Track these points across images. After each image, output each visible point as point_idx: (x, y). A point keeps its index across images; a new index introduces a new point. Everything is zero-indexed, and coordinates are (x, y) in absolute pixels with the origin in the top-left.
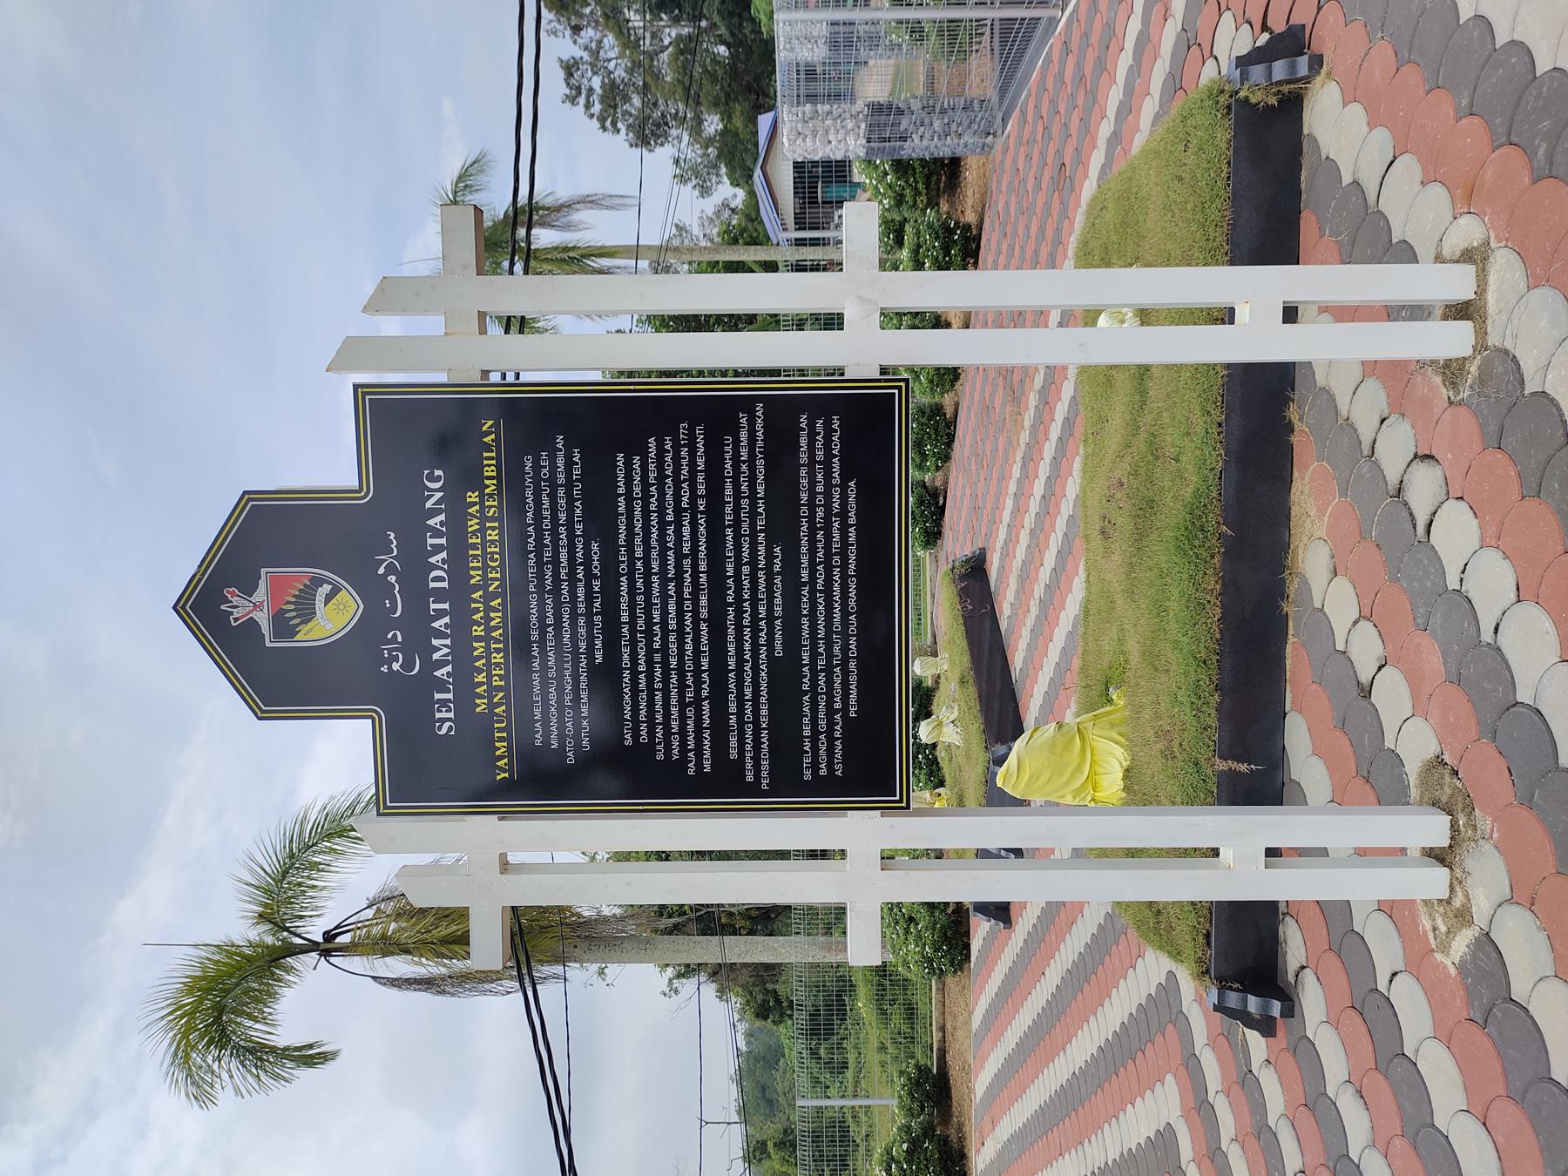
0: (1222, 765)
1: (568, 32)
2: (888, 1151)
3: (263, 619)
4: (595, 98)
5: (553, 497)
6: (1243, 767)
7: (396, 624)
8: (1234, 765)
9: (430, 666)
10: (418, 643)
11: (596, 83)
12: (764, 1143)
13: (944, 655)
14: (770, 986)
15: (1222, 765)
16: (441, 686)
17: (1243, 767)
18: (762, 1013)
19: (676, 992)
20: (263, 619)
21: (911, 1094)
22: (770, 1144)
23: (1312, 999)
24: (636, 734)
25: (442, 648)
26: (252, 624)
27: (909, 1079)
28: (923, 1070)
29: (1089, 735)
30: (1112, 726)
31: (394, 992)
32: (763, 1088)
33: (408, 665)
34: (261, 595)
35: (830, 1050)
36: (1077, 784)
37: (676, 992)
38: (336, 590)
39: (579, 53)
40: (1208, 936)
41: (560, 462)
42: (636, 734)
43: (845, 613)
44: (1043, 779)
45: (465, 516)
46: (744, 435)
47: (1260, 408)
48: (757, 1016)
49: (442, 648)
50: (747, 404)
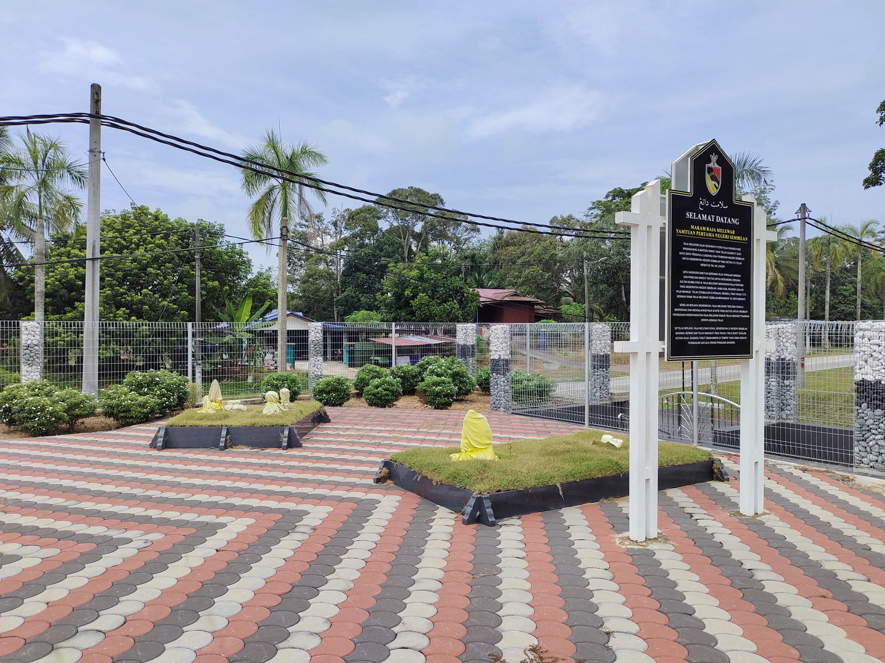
0: (558, 485)
1: (334, 220)
3: (711, 165)
4: (304, 229)
6: (561, 493)
8: (560, 488)
9: (701, 212)
10: (708, 211)
11: (311, 230)
16: (697, 216)
17: (561, 493)
20: (711, 165)
24: (686, 274)
25: (704, 217)
26: (710, 162)
33: (702, 207)
36: (473, 443)
39: (325, 222)
40: (500, 491)
42: (686, 274)
44: (475, 430)
49: (704, 217)
50: (749, 314)
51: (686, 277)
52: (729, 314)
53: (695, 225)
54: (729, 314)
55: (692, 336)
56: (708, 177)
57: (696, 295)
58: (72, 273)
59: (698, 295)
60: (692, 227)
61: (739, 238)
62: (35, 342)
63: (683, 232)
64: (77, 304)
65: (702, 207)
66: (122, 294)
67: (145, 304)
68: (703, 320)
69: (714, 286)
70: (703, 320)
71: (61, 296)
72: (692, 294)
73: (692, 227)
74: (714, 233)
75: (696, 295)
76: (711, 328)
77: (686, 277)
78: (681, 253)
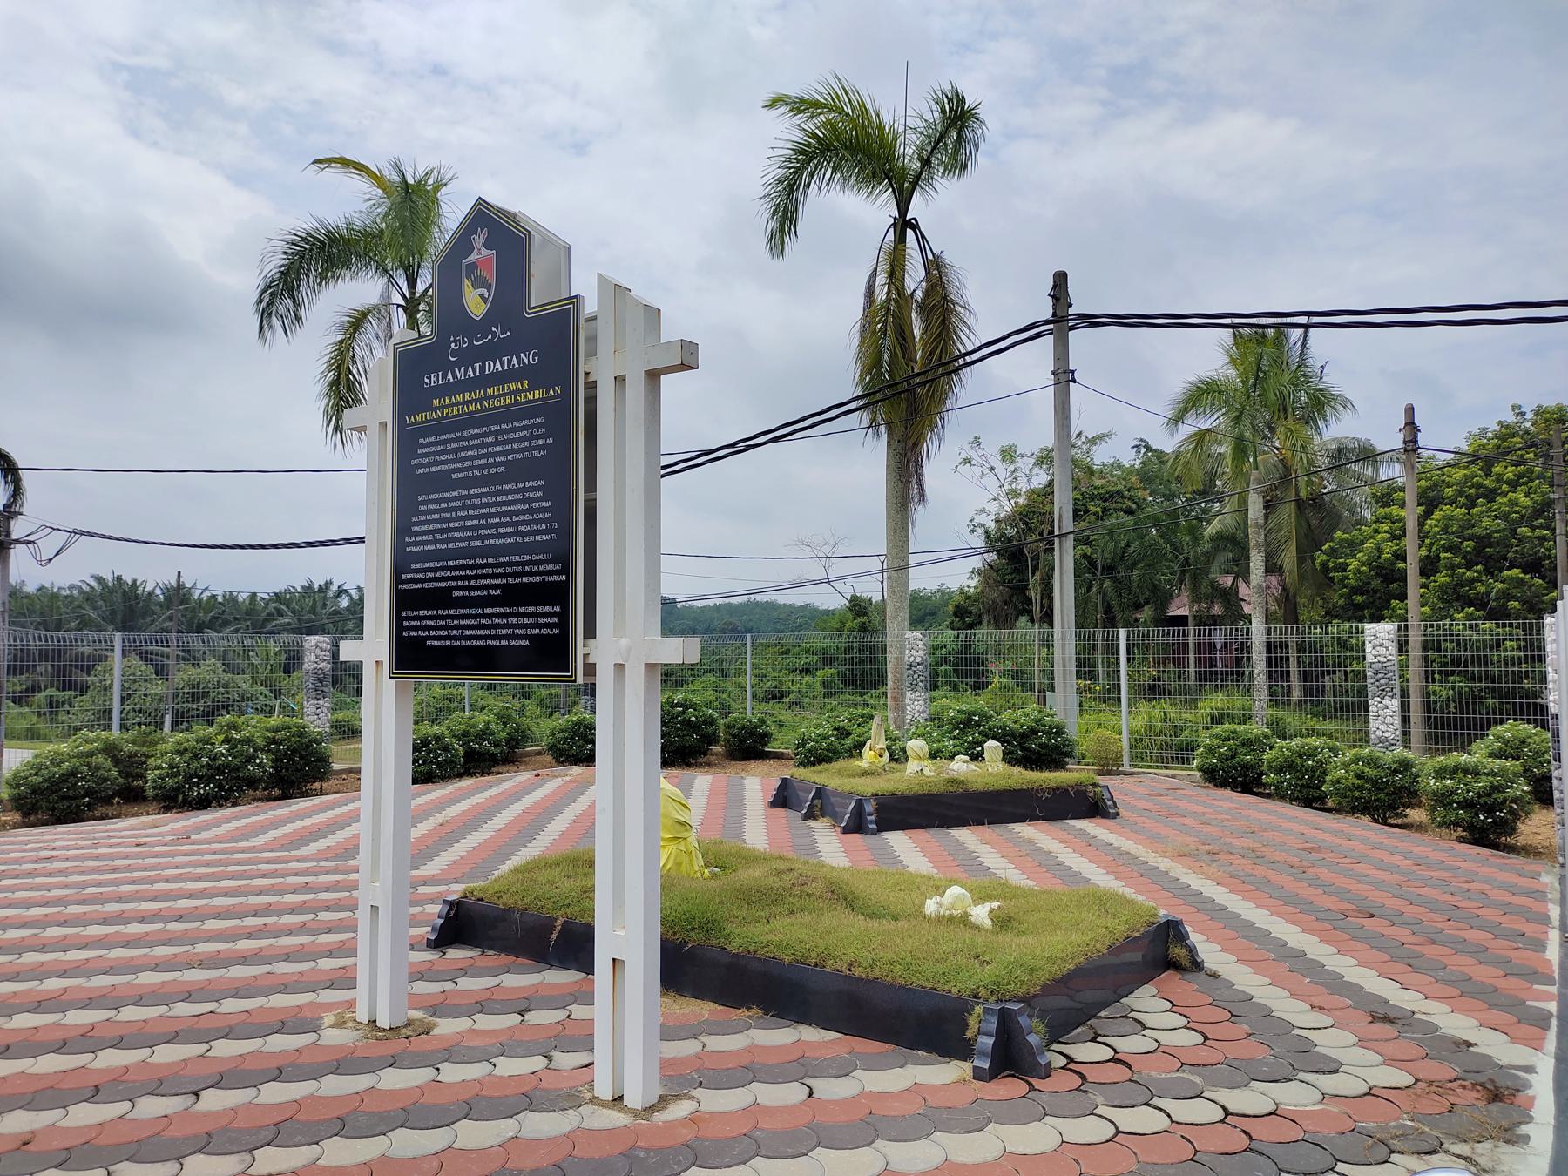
2: (694, 706)
5: (525, 439)
6: (554, 937)
7: (471, 342)
9: (453, 366)
10: (467, 358)
12: (865, 614)
13: (929, 769)
14: (985, 619)
15: (559, 922)
16: (445, 376)
17: (554, 937)
18: (960, 612)
19: (973, 531)
20: (474, 256)
21: (744, 727)
22: (864, 619)
23: (431, 956)
27: (756, 727)
28: (766, 738)
29: (673, 845)
30: (679, 864)
31: (862, 289)
32: (934, 614)
33: (454, 353)
34: (485, 252)
35: (945, 674)
37: (973, 531)
38: (485, 300)
41: (540, 442)
43: (470, 638)
45: (516, 381)
46: (551, 567)
47: (570, 945)
48: (957, 607)
51: (422, 508)
52: (515, 575)
53: (442, 396)
54: (515, 575)
55: (437, 630)
56: (466, 283)
57: (442, 542)
58: (1388, 549)
59: (447, 541)
60: (436, 403)
61: (538, 394)
62: (918, 660)
63: (418, 418)
64: (1394, 603)
65: (454, 353)
66: (1472, 581)
67: (1514, 598)
68: (456, 594)
69: (478, 517)
70: (456, 594)
71: (1375, 592)
72: (435, 542)
73: (436, 403)
74: (481, 400)
75: (442, 542)
76: (473, 611)
77: (422, 508)
78: (415, 462)
